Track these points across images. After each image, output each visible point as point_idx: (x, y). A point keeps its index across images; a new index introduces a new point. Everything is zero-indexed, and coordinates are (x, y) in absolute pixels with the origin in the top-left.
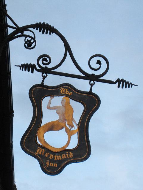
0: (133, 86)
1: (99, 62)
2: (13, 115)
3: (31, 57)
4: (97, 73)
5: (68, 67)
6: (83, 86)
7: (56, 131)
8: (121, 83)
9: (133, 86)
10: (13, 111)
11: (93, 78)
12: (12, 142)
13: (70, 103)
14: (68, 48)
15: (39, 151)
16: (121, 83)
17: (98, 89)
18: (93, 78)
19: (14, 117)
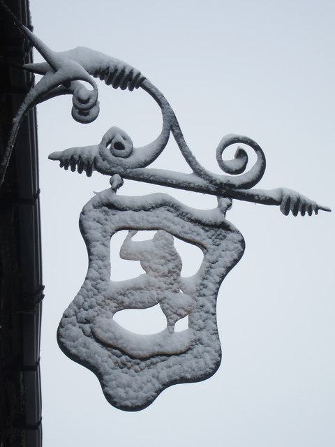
0: (319, 211)
1: (241, 154)
2: (43, 296)
3: (88, 137)
4: (236, 179)
5: (171, 162)
6: (204, 204)
7: (87, 48)
8: (295, 206)
9: (319, 211)
10: (43, 288)
11: (226, 191)
12: (39, 359)
13: (175, 245)
14: (172, 125)
15: (95, 274)
16: (295, 206)
17: (240, 214)
18: (226, 191)
19: (44, 301)
